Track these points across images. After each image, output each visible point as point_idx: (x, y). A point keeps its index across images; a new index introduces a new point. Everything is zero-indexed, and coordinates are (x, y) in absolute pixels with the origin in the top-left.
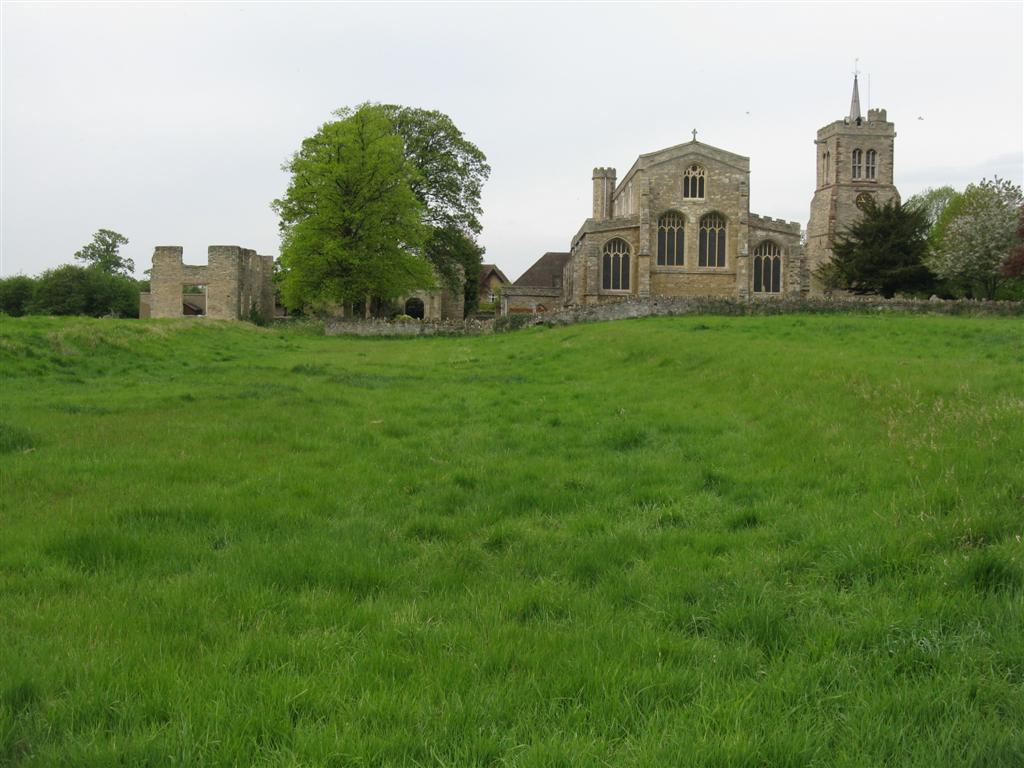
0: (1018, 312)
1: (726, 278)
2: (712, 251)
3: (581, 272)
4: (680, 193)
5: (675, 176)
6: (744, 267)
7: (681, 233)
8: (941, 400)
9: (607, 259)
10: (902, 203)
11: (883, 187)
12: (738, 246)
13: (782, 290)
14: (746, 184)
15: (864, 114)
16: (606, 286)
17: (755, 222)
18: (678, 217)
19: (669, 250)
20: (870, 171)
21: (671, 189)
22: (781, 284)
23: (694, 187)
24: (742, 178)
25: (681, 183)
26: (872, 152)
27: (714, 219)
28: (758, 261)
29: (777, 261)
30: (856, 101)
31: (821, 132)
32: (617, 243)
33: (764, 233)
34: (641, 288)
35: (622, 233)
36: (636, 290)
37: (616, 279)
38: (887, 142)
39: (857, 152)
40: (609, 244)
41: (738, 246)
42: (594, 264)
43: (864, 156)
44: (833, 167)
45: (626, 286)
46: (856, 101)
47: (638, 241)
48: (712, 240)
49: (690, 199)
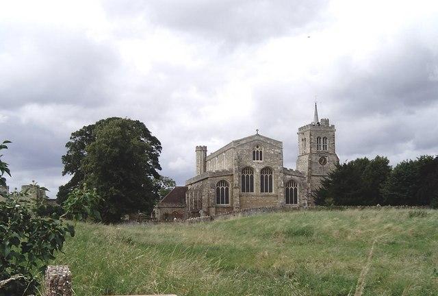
1: (273, 198)
2: (266, 186)
3: (206, 196)
5: (249, 151)
6: (282, 192)
8: (334, 235)
9: (218, 189)
12: (278, 183)
14: (281, 154)
16: (218, 203)
17: (286, 172)
18: (251, 170)
19: (247, 185)
20: (325, 147)
21: (247, 156)
23: (257, 156)
26: (325, 138)
28: (287, 189)
29: (296, 189)
32: (222, 182)
34: (235, 203)
36: (232, 205)
38: (332, 133)
39: (319, 138)
40: (219, 182)
41: (278, 183)
42: (213, 192)
43: (322, 140)
44: (308, 145)
45: (227, 203)
48: (266, 180)
49: (256, 161)
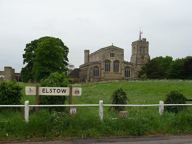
0: (191, 79)
2: (116, 69)
3: (89, 73)
4: (110, 56)
7: (110, 65)
10: (151, 59)
11: (146, 55)
12: (122, 67)
13: (130, 77)
14: (123, 55)
15: (142, 39)
16: (94, 76)
18: (110, 61)
19: (107, 69)
22: (130, 76)
23: (112, 55)
24: (121, 53)
25: (110, 54)
27: (117, 62)
29: (129, 71)
30: (140, 36)
31: (28, 45)
32: (96, 67)
33: (127, 65)
35: (97, 65)
37: (96, 74)
44: (136, 50)
45: (98, 76)
46: (140, 36)
47: (101, 66)
48: (116, 66)
